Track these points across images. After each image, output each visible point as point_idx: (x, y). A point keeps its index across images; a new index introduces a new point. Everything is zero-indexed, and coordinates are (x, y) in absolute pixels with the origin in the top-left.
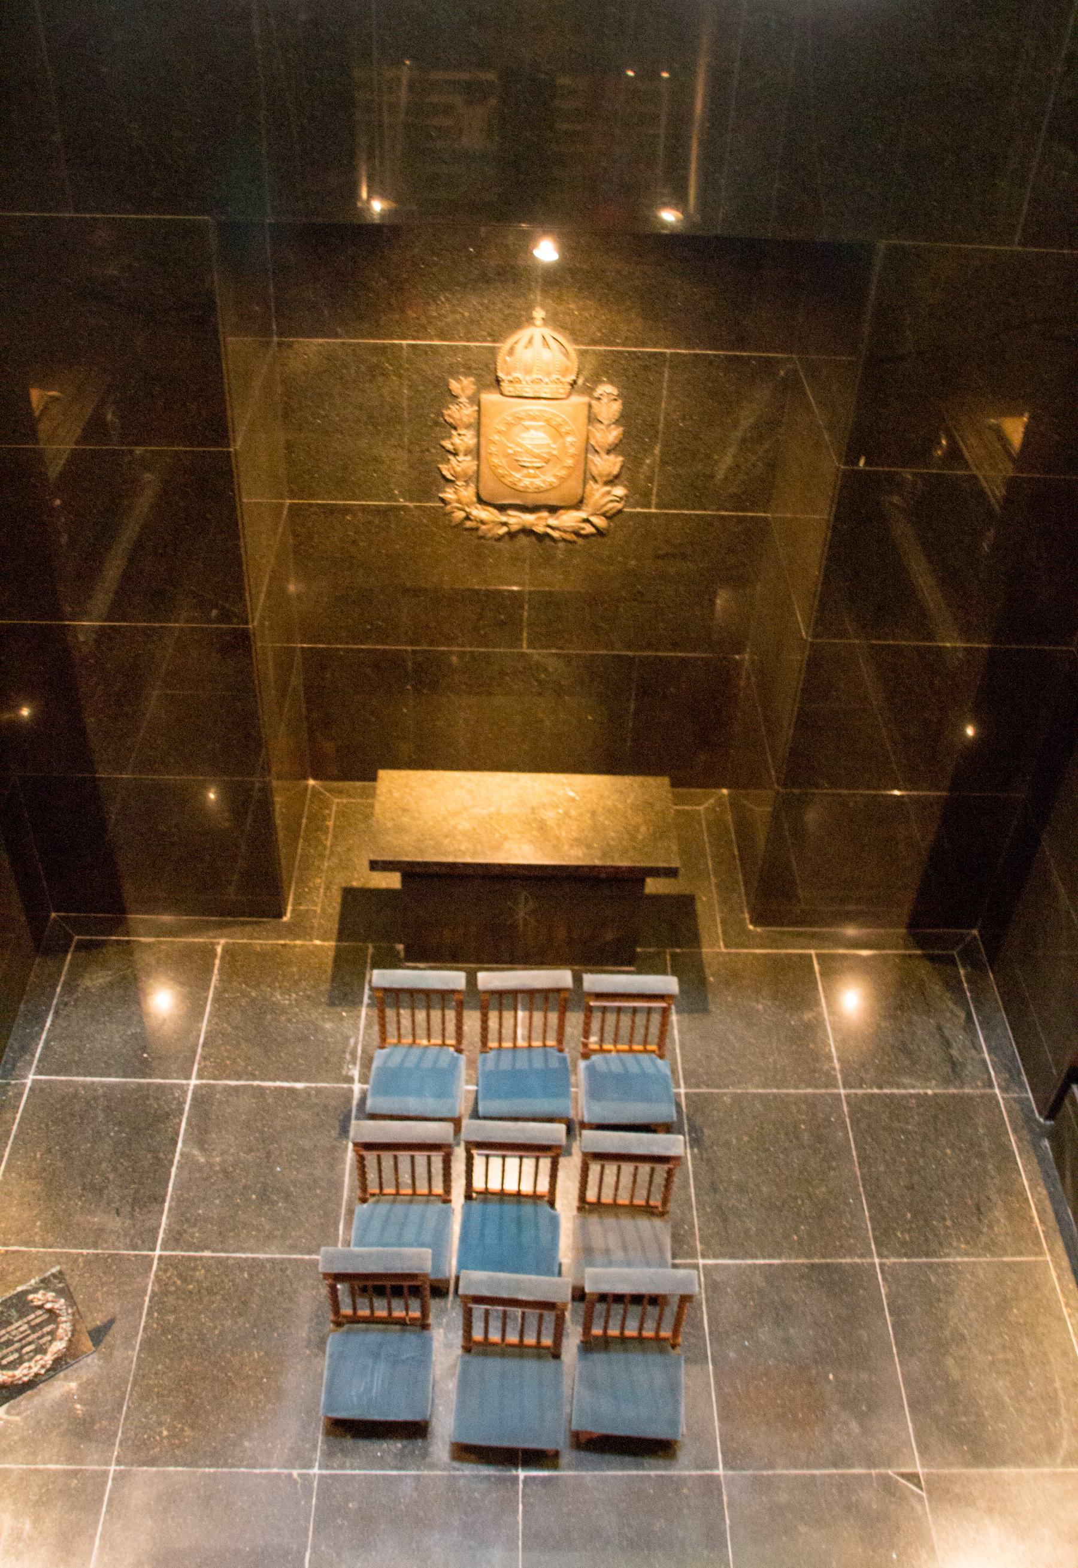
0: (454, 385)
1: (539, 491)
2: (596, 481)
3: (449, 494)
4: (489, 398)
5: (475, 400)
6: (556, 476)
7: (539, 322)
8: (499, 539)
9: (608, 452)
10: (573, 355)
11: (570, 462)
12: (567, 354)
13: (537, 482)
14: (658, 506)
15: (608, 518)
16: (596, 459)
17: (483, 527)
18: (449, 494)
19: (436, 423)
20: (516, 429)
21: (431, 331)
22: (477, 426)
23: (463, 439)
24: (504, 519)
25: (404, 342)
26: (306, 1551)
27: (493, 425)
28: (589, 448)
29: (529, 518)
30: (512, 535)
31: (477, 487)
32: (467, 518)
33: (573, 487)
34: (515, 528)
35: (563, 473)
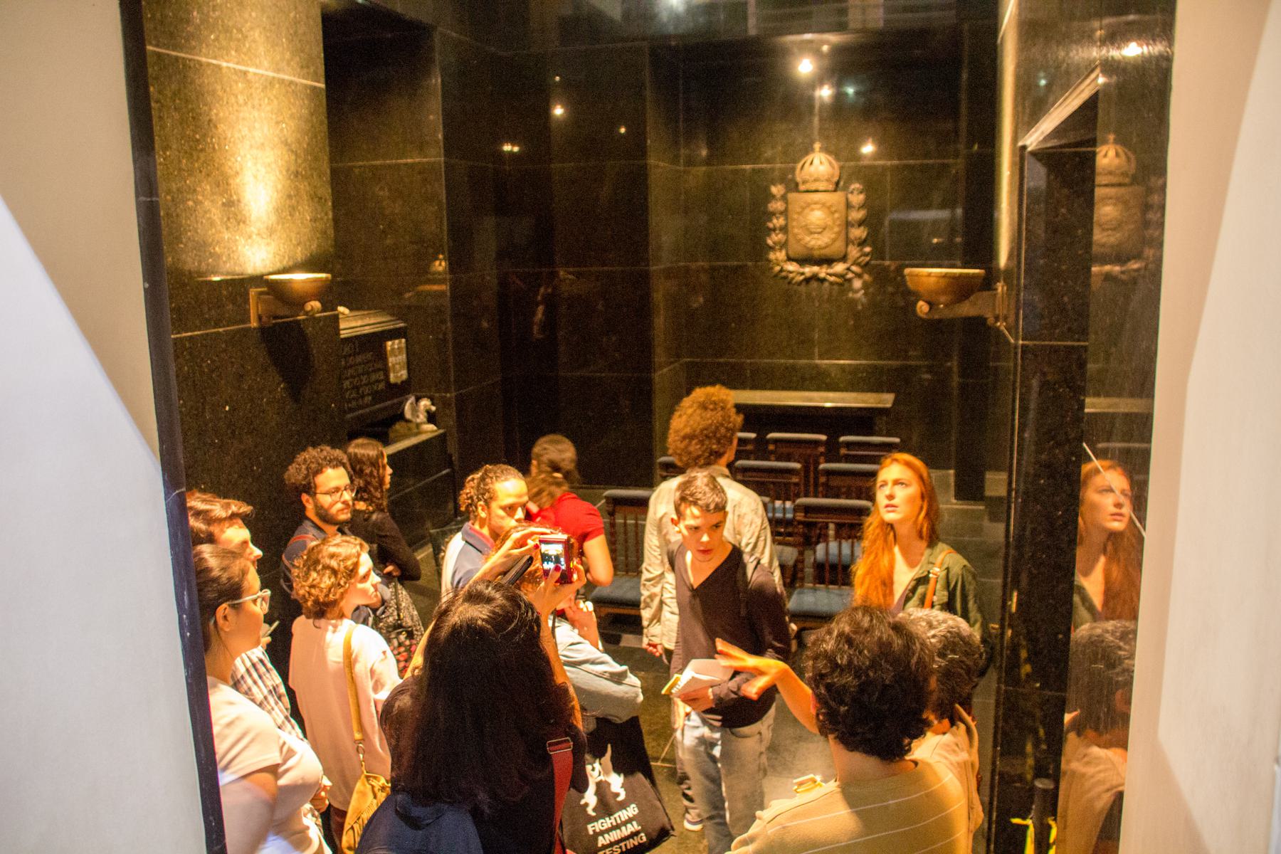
1: (820, 248)
3: (772, 256)
4: (792, 196)
5: (784, 198)
8: (800, 283)
9: (860, 226)
11: (836, 229)
13: (820, 243)
15: (862, 267)
18: (772, 256)
20: (807, 211)
22: (785, 213)
23: (778, 222)
24: (801, 270)
26: (693, 562)
28: (848, 225)
29: (816, 269)
30: (807, 280)
32: (782, 270)
33: (838, 247)
34: (808, 275)
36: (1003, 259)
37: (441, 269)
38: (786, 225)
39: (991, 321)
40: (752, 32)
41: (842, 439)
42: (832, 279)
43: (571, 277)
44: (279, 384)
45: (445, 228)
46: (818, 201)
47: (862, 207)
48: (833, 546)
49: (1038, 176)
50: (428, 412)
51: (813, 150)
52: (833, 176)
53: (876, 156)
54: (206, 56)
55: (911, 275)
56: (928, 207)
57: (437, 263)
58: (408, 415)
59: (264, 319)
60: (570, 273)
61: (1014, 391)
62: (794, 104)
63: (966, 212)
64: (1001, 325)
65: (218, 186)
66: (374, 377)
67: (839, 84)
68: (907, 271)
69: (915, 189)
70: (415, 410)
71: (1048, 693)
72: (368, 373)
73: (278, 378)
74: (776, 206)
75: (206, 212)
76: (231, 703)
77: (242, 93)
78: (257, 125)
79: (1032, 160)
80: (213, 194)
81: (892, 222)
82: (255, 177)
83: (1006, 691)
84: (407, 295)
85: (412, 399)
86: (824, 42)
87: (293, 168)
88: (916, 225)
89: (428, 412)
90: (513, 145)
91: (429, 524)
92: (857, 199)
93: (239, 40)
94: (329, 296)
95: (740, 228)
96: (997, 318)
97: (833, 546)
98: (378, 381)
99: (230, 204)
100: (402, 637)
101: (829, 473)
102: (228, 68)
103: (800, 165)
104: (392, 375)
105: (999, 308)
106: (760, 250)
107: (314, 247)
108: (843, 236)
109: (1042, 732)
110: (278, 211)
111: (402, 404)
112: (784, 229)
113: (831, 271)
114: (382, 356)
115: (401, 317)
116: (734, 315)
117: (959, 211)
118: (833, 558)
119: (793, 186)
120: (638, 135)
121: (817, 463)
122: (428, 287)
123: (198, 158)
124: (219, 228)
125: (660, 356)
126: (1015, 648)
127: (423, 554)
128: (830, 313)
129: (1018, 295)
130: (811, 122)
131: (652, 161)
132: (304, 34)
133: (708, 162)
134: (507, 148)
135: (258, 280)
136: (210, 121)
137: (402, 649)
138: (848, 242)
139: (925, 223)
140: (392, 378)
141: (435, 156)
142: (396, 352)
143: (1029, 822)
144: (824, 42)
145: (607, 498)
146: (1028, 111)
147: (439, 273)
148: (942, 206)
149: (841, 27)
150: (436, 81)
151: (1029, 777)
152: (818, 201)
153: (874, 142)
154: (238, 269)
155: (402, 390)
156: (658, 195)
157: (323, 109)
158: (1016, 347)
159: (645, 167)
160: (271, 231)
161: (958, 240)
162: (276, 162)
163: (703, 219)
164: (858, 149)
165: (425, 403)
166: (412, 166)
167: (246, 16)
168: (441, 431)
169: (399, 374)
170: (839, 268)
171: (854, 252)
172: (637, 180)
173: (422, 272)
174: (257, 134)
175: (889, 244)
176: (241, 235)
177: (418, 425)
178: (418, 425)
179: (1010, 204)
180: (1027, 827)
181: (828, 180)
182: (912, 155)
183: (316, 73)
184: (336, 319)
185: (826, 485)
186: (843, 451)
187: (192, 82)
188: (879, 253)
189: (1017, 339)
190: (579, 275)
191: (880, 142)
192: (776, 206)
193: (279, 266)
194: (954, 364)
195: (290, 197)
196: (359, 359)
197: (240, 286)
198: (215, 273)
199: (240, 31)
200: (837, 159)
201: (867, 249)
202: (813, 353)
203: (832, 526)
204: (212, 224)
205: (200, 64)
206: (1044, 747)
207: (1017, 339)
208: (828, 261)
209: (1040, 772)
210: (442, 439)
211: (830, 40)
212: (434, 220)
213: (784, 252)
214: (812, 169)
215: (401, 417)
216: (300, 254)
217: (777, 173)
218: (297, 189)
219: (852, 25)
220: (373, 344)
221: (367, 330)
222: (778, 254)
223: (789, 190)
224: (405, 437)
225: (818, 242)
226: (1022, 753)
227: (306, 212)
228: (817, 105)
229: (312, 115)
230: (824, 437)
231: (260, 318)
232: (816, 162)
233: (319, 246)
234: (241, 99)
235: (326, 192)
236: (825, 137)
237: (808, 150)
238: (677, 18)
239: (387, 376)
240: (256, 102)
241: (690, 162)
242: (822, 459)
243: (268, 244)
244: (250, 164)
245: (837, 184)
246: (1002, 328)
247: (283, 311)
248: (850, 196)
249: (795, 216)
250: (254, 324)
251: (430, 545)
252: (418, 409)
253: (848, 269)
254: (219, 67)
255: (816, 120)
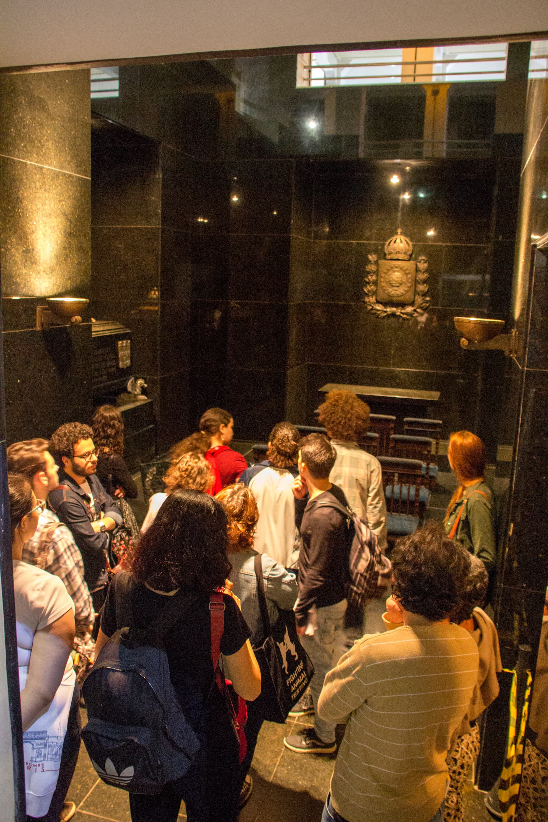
0: (370, 257)
1: (398, 296)
2: (419, 295)
3: (367, 299)
4: (381, 262)
5: (376, 263)
6: (404, 290)
7: (399, 233)
8: (384, 318)
10: (411, 245)
11: (409, 285)
12: (409, 245)
13: (397, 293)
14: (442, 306)
16: (419, 286)
17: (378, 313)
19: (363, 272)
20: (390, 272)
21: (364, 238)
22: (376, 273)
24: (385, 310)
25: (354, 242)
27: (383, 269)
28: (416, 282)
29: (394, 309)
30: (388, 316)
31: (376, 297)
32: (372, 309)
33: (409, 296)
34: (389, 313)
35: (406, 289)
36: (517, 314)
37: (155, 296)
38: (377, 280)
39: (507, 353)
40: (361, 155)
41: (406, 419)
42: (404, 316)
43: (238, 306)
44: (52, 367)
45: (159, 271)
46: (398, 266)
47: (426, 271)
48: (397, 488)
49: (541, 260)
50: (142, 387)
51: (396, 233)
52: (408, 250)
53: (436, 239)
54: (18, 157)
55: (458, 321)
56: (469, 273)
57: (153, 293)
58: (129, 389)
59: (45, 325)
60: (237, 303)
61: (520, 399)
62: (387, 202)
63: (492, 277)
64: (513, 356)
65: (21, 240)
66: (109, 364)
67: (414, 193)
68: (456, 318)
69: (461, 260)
70: (134, 386)
71: (530, 590)
72: (105, 361)
73: (51, 364)
74: (372, 267)
75: (12, 256)
76: (38, 575)
77: (39, 181)
78: (47, 202)
79: (540, 253)
80: (18, 244)
81: (444, 281)
82: (44, 235)
83: (504, 588)
84: (132, 312)
85: (132, 379)
86: (407, 165)
87: (68, 230)
88: (460, 284)
89: (142, 387)
90: (204, 219)
91: (139, 460)
92: (423, 266)
93: (39, 147)
94: (87, 312)
95: (348, 280)
96: (511, 352)
97: (397, 488)
98: (112, 367)
99: (27, 251)
100: (124, 534)
101: (396, 441)
102: (31, 165)
103: (388, 242)
104: (120, 363)
105: (512, 345)
106: (359, 295)
107: (78, 281)
108: (412, 290)
109: (525, 615)
110: (57, 256)
111: (126, 381)
112: (375, 283)
113: (403, 311)
114: (115, 350)
115: (127, 326)
116: (341, 336)
117: (488, 277)
118: (396, 496)
119: (382, 255)
120: (285, 216)
121: (389, 434)
122: (146, 308)
123: (9, 221)
124: (20, 266)
125: (291, 360)
126: (510, 561)
127: (136, 477)
128: (402, 338)
129: (526, 339)
130: (396, 216)
131: (293, 235)
132: (80, 145)
133: (329, 237)
134: (200, 220)
135: (43, 300)
136: (18, 198)
137: (123, 542)
138: (416, 293)
139: (465, 282)
140: (121, 365)
141: (156, 225)
142: (124, 349)
143: (514, 671)
144: (407, 165)
145: (254, 449)
146: (539, 224)
147: (154, 299)
148: (477, 273)
149: (418, 156)
150: (159, 176)
151: (515, 643)
152: (398, 266)
153: (435, 230)
154: (30, 293)
155: (126, 373)
156: (295, 256)
157: (89, 193)
158: (523, 372)
159: (289, 237)
160: (52, 270)
161: (486, 294)
162: (57, 226)
163: (324, 272)
164: (426, 233)
165: (140, 382)
166: (140, 229)
167: (44, 133)
168: (150, 400)
169: (125, 362)
170: (409, 309)
171: (419, 300)
172: (283, 247)
173: (143, 297)
174: (47, 207)
175: (444, 299)
176: (33, 271)
177: (135, 396)
178: (135, 396)
179: (524, 280)
180: (513, 674)
181: (405, 253)
182: (460, 240)
183: (86, 170)
184: (89, 327)
185: (394, 448)
186: (406, 427)
187: (8, 173)
188: (435, 301)
189: (523, 367)
190: (242, 305)
191: (440, 230)
192: (372, 267)
193: (56, 292)
194: (479, 374)
195: (65, 248)
196: (100, 352)
197: (32, 303)
198: (16, 295)
199: (40, 142)
200: (412, 240)
201: (428, 299)
202: (389, 363)
203: (396, 475)
204: (16, 263)
205: (14, 161)
206: (525, 624)
207: (523, 367)
208: (402, 305)
209: (523, 640)
210: (151, 404)
211: (410, 164)
212: (152, 264)
213: (374, 298)
214: (395, 245)
215: (125, 390)
216: (69, 285)
217: (372, 247)
218: (70, 243)
219: (425, 154)
220: (109, 342)
221: (107, 333)
222: (371, 298)
223: (379, 258)
224: (125, 403)
225: (397, 292)
226: (512, 629)
227: (75, 258)
228: (401, 204)
229: (82, 196)
230: (394, 418)
231: (42, 325)
232: (398, 241)
233: (81, 281)
234: (38, 184)
235: (88, 246)
236: (405, 226)
237: (393, 233)
238: (314, 144)
239: (117, 363)
240: (47, 187)
241: (318, 236)
242: (392, 432)
243: (50, 278)
244: (41, 226)
245: (411, 256)
246: (514, 358)
247: (58, 321)
248: (418, 264)
249: (383, 275)
250: (38, 328)
251: (139, 473)
252: (136, 385)
253: (415, 311)
254: (26, 164)
255: (399, 214)
